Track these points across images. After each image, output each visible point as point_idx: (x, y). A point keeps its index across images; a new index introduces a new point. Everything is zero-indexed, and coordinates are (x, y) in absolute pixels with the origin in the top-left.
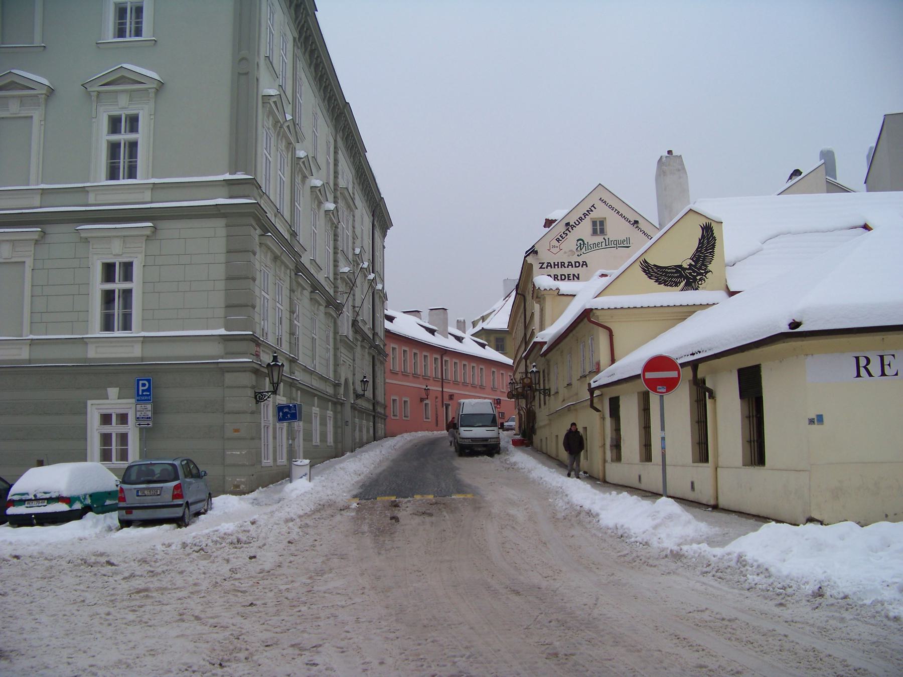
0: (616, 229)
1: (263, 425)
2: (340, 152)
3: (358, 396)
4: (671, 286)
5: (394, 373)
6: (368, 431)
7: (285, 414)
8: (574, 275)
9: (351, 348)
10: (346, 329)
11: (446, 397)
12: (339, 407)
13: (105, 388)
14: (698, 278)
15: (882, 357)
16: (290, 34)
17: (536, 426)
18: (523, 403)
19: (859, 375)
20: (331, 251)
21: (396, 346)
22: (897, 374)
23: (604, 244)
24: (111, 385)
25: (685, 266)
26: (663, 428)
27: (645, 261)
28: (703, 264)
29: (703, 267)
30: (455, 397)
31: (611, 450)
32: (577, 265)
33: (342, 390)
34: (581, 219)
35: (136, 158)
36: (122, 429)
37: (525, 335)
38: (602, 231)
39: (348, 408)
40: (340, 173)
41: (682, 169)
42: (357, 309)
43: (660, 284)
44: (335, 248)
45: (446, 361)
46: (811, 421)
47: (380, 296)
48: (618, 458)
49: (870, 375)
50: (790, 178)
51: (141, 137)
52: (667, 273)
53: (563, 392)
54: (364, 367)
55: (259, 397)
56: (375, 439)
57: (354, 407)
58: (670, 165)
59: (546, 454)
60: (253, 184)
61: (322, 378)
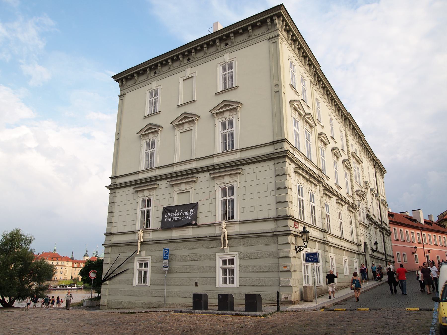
2: (349, 136)
3: (374, 251)
5: (396, 240)
11: (426, 251)
16: (308, 78)
26: (341, 224)
36: (231, 267)
45: (424, 234)
57: (371, 257)
61: (348, 241)
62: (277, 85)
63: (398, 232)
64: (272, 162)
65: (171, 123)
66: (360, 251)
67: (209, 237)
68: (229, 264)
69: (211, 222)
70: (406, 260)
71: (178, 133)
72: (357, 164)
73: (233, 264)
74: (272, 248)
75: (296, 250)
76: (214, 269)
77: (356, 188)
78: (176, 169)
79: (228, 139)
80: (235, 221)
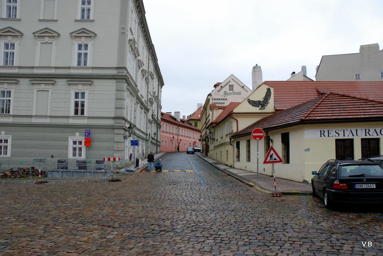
0: (237, 89)
1: (126, 146)
2: (150, 60)
3: (153, 139)
4: (257, 107)
5: (163, 132)
6: (155, 150)
7: (133, 143)
8: (223, 103)
9: (151, 123)
10: (150, 117)
11: (179, 140)
12: (147, 142)
13: (75, 133)
14: (265, 105)
15: (328, 131)
16: (137, 21)
17: (209, 150)
18: (204, 143)
19: (321, 136)
20: (146, 92)
21: (164, 123)
22: (333, 136)
23: (232, 93)
24: (76, 132)
25: (261, 101)
27: (249, 99)
28: (267, 101)
29: (267, 102)
30: (182, 140)
31: (236, 158)
32: (224, 99)
33: (148, 136)
34: (226, 85)
35: (87, 58)
36: (80, 146)
37: (206, 121)
38: (232, 90)
39: (149, 142)
40: (150, 67)
41: (261, 71)
42: (153, 111)
43: (253, 106)
44: (148, 91)
45: (179, 129)
46: (306, 150)
47: (160, 107)
48: (239, 160)
49: (325, 136)
50: (292, 74)
51: (89, 51)
52: (256, 103)
53: (220, 140)
54: (154, 129)
55: (125, 138)
56: (157, 153)
57: (151, 142)
58: (256, 69)
59: (213, 159)
60: (125, 69)
62: (123, 28)
63: (165, 126)
64: (114, 81)
65: (33, 33)
66: (147, 138)
67: (64, 125)
68: (4, 143)
69: (66, 115)
70: (167, 145)
71: (39, 42)
72: (151, 79)
73: (7, 142)
74: (110, 136)
75: (124, 138)
76: (67, 148)
77: (150, 97)
78: (36, 71)
79: (82, 58)
80: (85, 116)
